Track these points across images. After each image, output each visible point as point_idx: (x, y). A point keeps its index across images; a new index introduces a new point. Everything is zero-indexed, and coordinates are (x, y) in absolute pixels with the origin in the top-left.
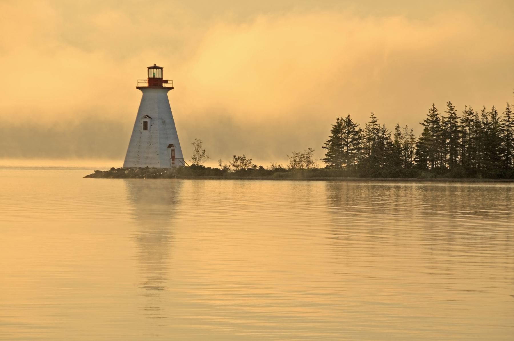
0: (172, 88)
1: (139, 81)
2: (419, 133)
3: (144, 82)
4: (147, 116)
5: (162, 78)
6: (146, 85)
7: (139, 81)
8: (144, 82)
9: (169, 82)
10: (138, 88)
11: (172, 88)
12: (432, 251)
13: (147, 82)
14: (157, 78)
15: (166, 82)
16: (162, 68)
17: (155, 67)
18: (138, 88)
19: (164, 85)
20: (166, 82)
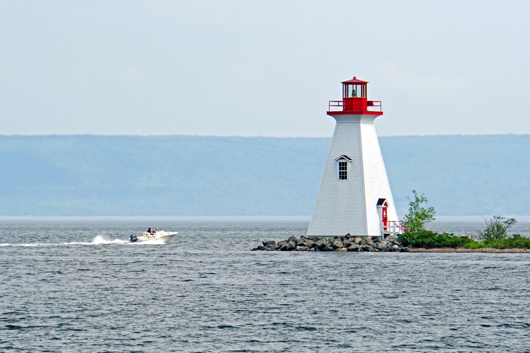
0: (381, 113)
1: (331, 104)
2: (361, 121)
3: (337, 104)
4: (345, 156)
5: (366, 99)
6: (341, 109)
7: (331, 104)
8: (337, 104)
9: (374, 104)
10: (329, 113)
11: (381, 113)
12: (11, 324)
13: (341, 104)
14: (350, 98)
15: (371, 104)
16: (365, 83)
17: (355, 82)
18: (329, 113)
19: (370, 109)
20: (371, 104)
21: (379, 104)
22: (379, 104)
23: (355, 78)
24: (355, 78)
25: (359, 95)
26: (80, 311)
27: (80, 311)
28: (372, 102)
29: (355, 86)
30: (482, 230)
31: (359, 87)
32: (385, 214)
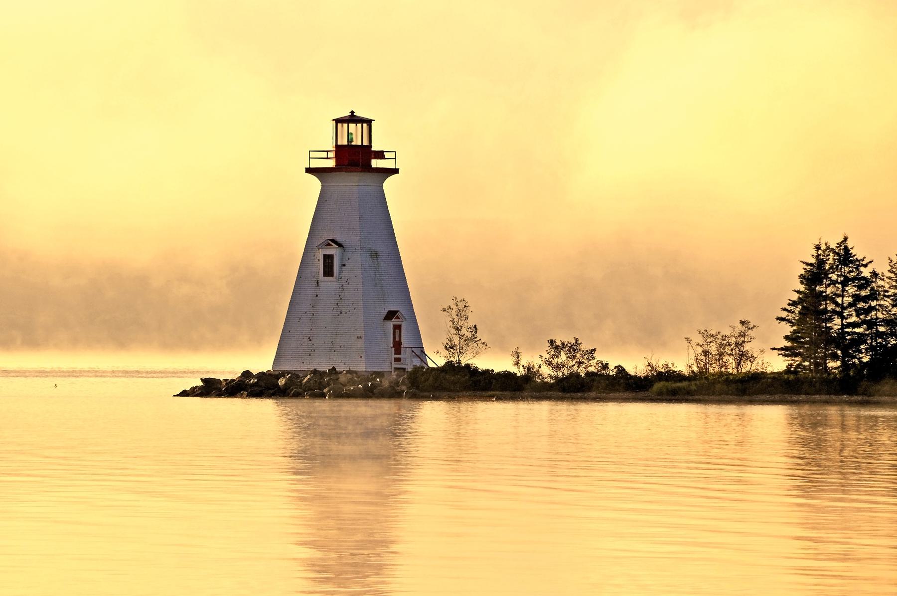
0: (395, 171)
1: (313, 155)
3: (324, 155)
5: (370, 146)
6: (331, 163)
7: (313, 155)
8: (324, 155)
10: (309, 170)
11: (395, 171)
13: (331, 155)
15: (380, 155)
16: (369, 122)
17: (353, 119)
18: (309, 170)
19: (376, 163)
20: (380, 155)
21: (392, 155)
22: (392, 155)
23: (352, 112)
24: (352, 112)
25: (357, 142)
26: (789, 321)
27: (789, 321)
28: (382, 152)
29: (359, 125)
30: (282, 428)
31: (365, 125)
32: (109, 374)
